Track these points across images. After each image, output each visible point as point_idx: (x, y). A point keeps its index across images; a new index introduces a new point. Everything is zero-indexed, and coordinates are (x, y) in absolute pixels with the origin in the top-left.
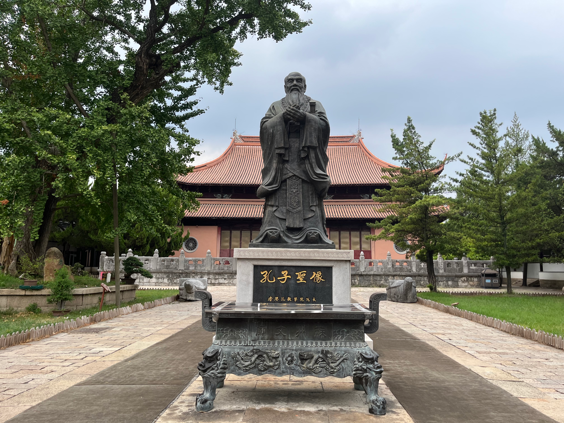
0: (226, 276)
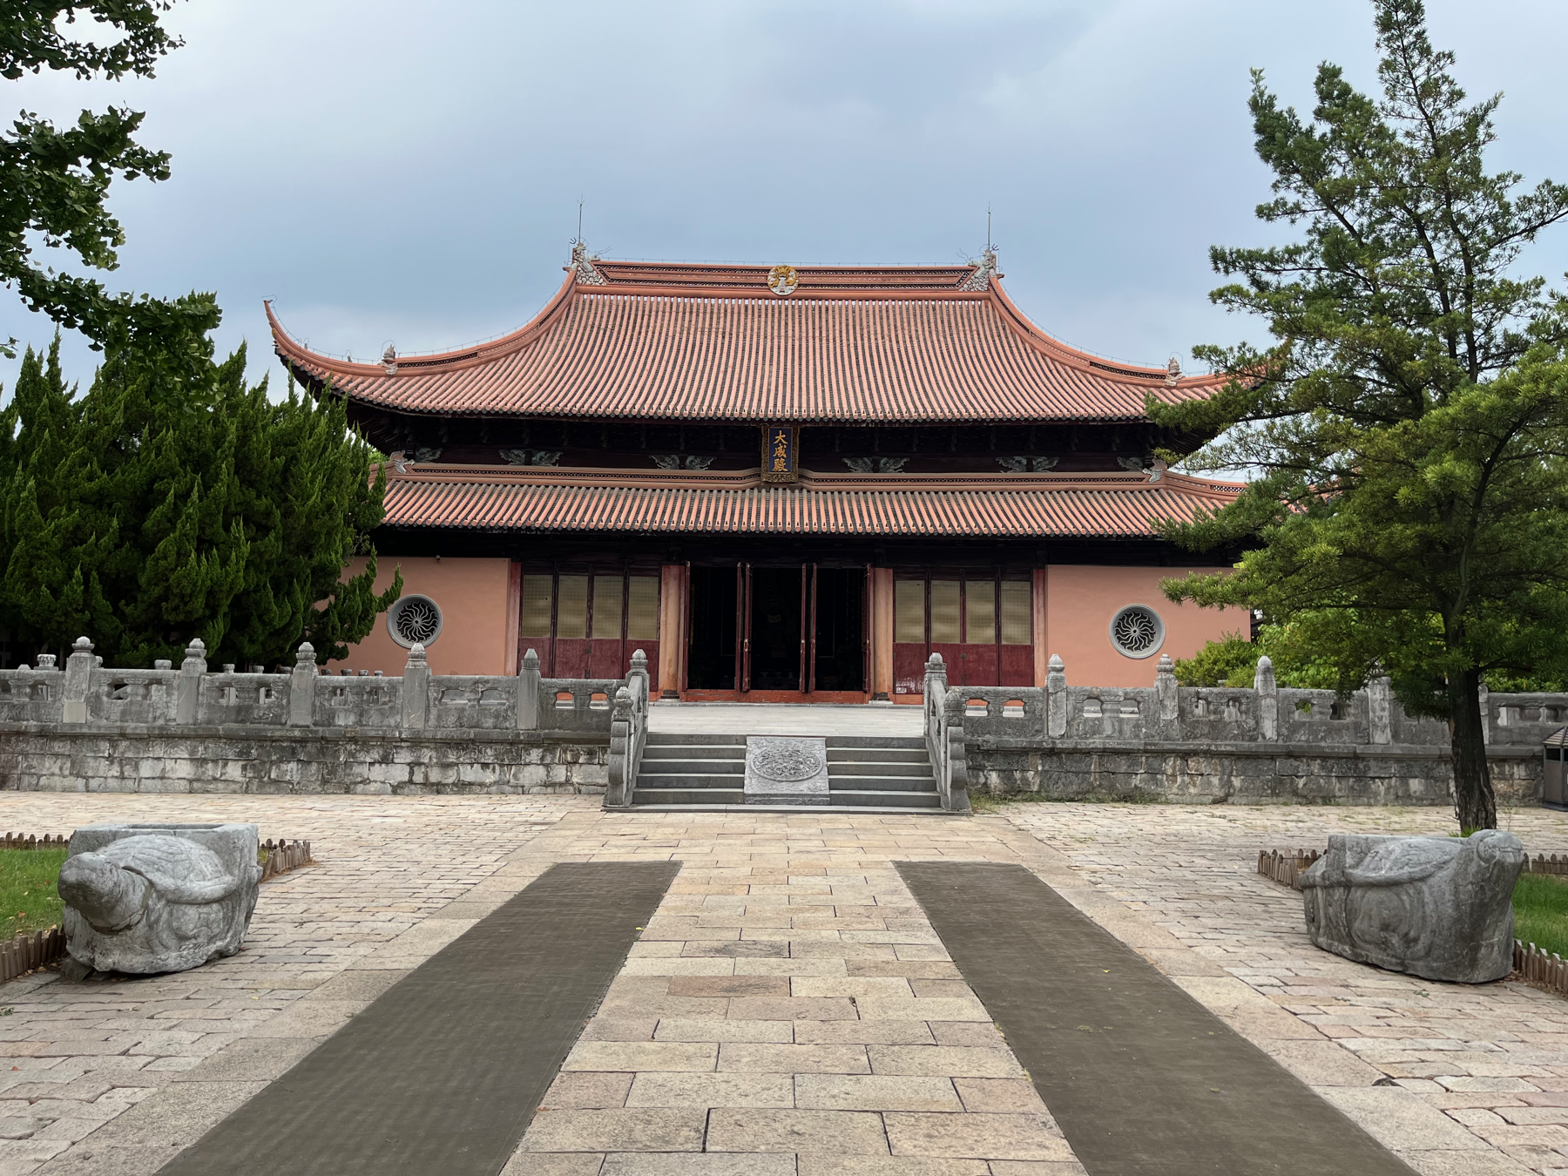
0: (489, 755)
